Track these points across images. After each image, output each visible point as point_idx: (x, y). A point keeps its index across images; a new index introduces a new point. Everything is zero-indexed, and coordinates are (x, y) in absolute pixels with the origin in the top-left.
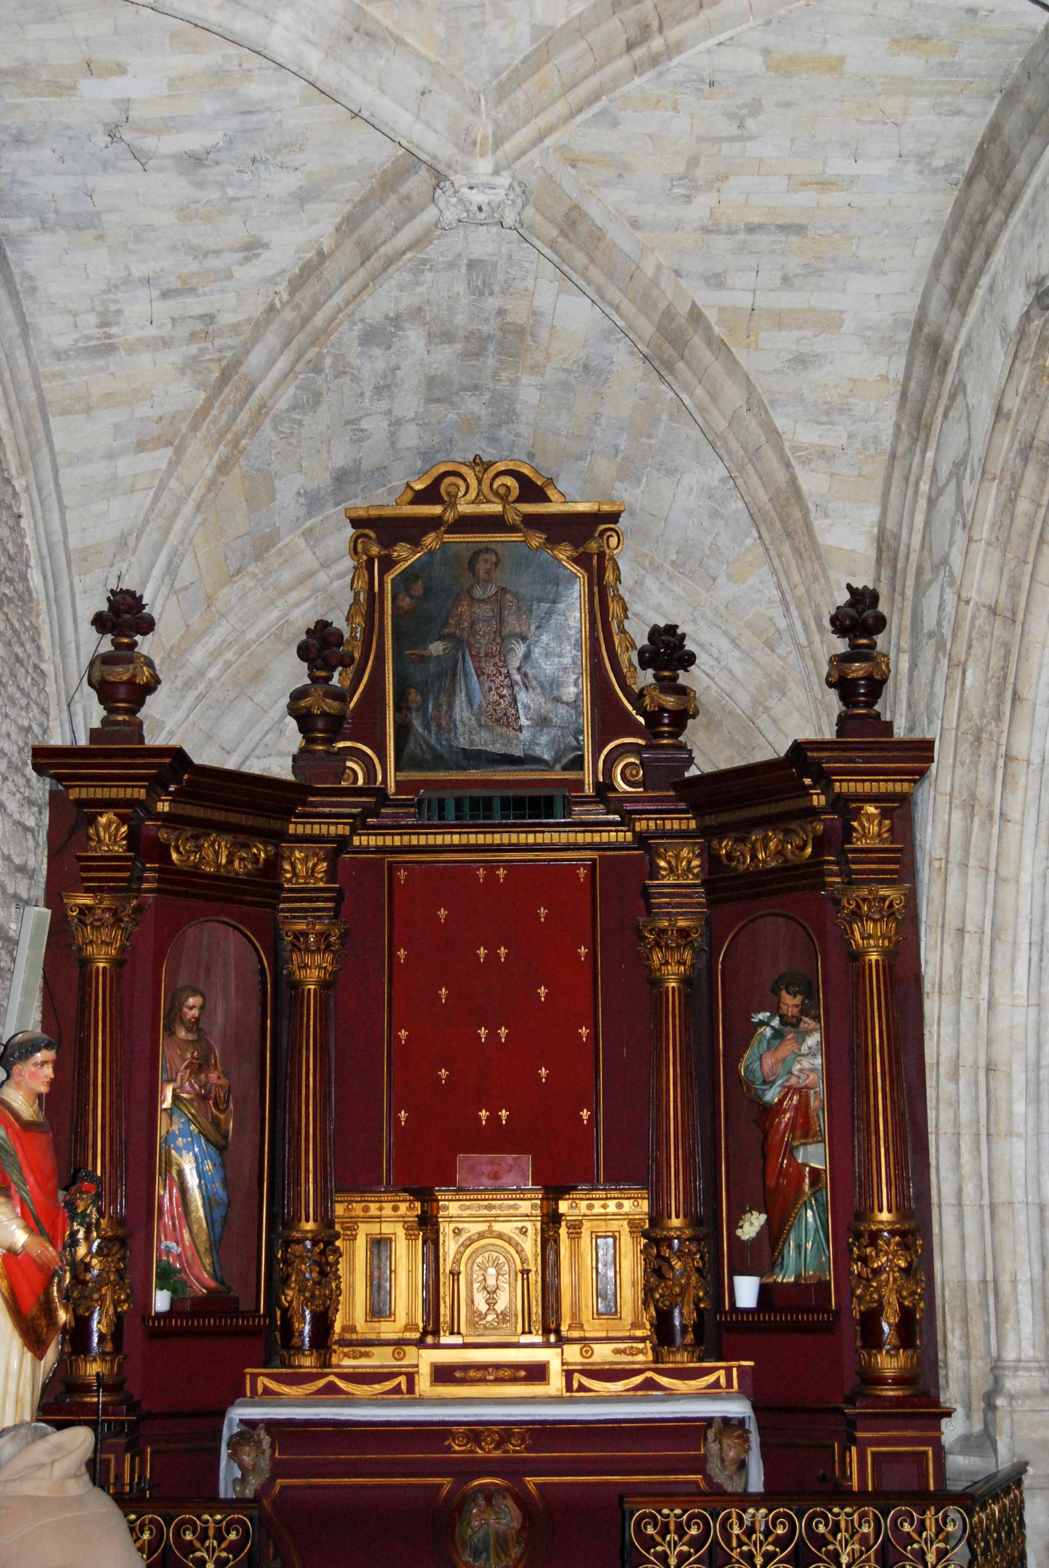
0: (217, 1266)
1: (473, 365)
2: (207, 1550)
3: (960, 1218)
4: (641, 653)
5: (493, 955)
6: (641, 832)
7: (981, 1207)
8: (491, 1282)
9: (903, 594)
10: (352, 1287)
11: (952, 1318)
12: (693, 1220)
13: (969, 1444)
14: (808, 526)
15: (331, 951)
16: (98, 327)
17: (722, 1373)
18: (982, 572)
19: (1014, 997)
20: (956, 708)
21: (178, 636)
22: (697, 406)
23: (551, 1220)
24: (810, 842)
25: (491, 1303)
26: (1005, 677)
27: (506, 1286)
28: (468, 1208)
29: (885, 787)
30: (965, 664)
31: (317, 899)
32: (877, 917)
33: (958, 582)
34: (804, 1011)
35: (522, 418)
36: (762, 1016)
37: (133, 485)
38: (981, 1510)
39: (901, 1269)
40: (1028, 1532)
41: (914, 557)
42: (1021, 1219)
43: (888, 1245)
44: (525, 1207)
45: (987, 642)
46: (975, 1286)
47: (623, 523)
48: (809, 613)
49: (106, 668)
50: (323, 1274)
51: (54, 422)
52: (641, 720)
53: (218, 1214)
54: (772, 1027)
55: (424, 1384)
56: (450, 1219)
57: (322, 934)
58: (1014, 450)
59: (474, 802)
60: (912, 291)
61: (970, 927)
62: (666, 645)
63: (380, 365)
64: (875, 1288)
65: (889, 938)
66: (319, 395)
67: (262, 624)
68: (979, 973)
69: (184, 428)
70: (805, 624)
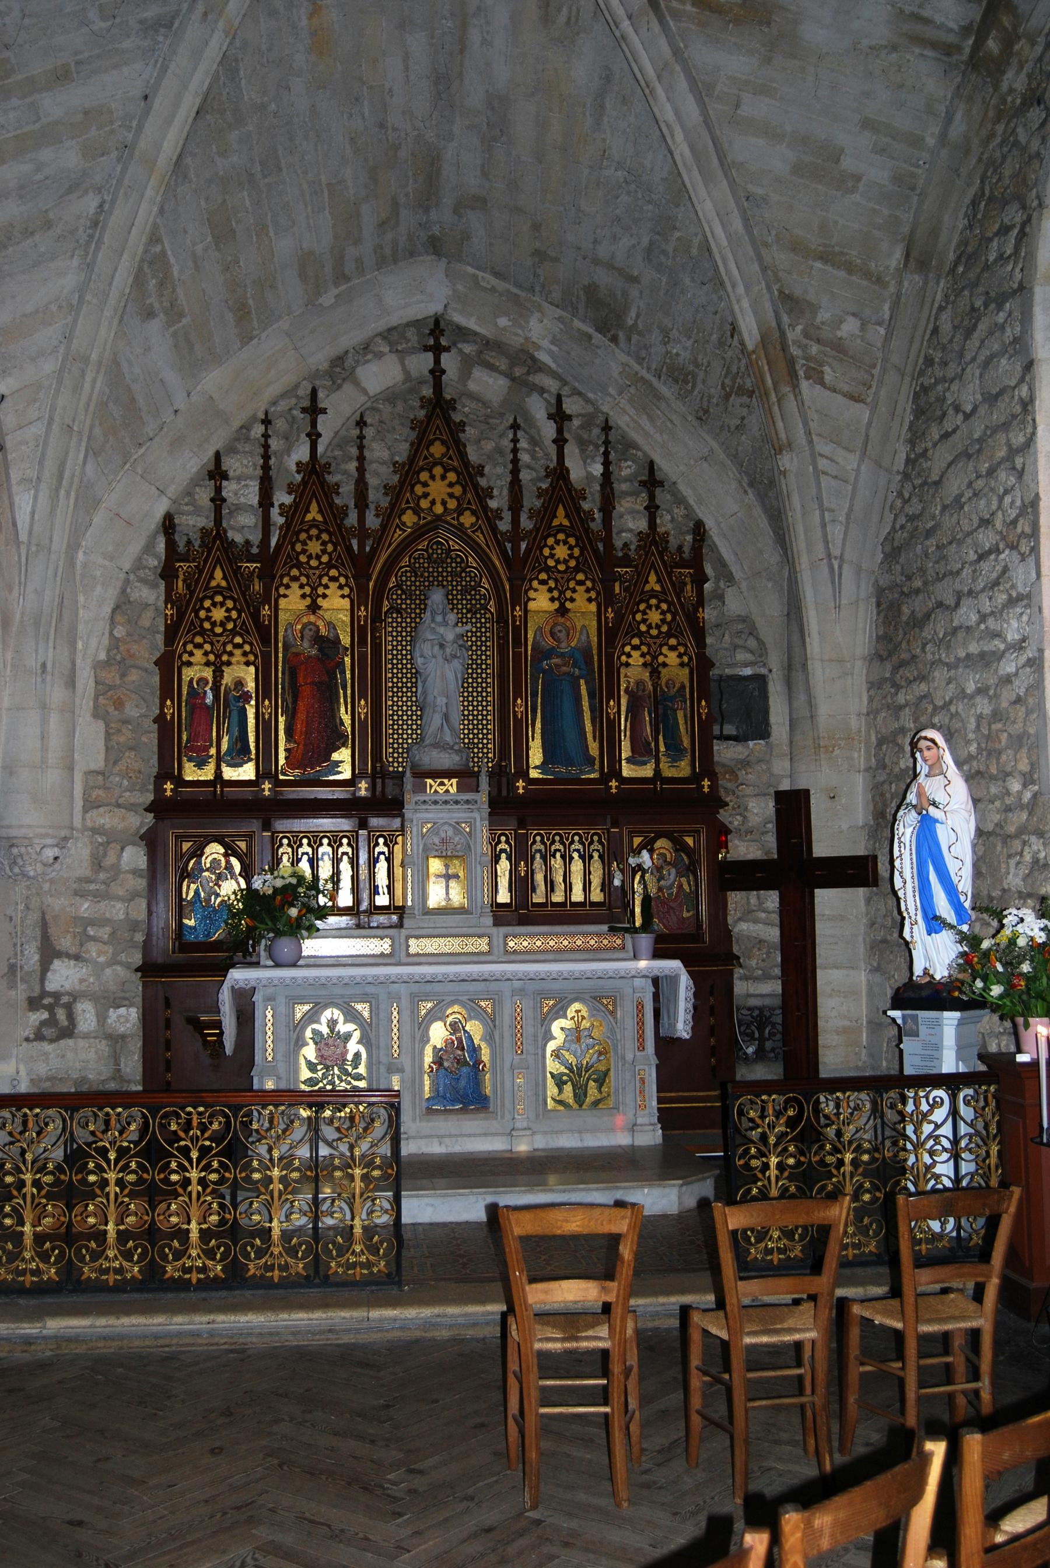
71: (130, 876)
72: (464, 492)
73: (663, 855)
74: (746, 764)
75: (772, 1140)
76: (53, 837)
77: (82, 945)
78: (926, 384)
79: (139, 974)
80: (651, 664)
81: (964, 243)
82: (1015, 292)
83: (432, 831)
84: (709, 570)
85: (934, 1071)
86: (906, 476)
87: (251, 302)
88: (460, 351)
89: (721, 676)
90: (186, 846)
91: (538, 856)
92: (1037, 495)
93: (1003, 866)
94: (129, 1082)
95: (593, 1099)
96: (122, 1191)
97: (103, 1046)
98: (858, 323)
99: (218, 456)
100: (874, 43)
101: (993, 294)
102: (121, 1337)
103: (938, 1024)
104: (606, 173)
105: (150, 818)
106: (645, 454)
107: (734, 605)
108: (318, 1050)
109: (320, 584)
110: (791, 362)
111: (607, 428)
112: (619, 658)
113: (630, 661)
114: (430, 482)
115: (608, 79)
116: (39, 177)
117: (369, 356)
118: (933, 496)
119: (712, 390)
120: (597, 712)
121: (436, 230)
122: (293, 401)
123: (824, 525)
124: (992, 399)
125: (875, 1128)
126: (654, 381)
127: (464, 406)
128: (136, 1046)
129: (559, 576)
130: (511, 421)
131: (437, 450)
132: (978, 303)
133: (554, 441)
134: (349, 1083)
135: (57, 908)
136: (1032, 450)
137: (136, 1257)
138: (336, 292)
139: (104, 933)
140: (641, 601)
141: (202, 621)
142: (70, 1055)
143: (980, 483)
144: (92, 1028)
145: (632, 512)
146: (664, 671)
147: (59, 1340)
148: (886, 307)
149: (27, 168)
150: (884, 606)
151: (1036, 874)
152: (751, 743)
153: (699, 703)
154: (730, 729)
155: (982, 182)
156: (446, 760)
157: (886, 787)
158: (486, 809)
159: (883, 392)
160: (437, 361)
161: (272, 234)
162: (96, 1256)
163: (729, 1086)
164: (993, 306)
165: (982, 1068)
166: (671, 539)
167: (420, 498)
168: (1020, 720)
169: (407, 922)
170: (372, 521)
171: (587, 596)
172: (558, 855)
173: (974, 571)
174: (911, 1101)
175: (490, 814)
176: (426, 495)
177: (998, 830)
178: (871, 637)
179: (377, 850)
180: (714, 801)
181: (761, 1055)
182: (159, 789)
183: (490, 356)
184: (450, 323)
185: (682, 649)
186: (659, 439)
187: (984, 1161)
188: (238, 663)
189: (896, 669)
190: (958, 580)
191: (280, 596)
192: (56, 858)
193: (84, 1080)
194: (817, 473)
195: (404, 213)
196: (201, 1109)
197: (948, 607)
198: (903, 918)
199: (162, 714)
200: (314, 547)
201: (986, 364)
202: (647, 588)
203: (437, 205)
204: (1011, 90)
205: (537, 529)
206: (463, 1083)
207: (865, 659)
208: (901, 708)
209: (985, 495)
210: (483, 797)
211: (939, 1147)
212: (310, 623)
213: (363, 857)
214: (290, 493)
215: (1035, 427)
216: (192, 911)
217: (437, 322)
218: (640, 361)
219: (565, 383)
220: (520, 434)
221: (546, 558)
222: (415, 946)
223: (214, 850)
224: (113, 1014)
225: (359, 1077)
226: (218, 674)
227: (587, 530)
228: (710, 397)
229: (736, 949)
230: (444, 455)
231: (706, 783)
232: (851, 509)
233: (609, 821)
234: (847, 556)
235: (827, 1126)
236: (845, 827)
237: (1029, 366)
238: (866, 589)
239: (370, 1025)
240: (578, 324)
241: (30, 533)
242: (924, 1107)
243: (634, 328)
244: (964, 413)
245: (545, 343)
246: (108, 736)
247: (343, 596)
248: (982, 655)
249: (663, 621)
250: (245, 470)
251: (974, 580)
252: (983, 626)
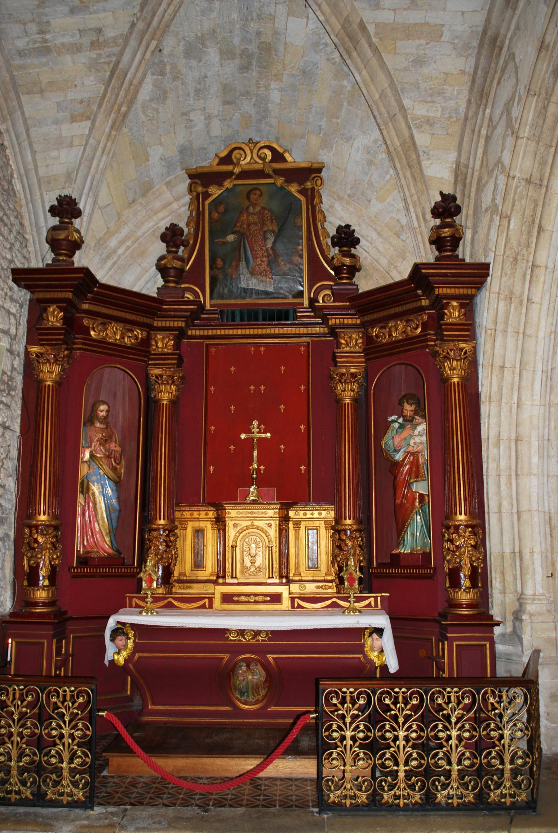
0: (114, 542)
1: (245, 77)
2: (66, 707)
3: (500, 519)
4: (333, 238)
5: (257, 390)
6: (332, 325)
7: (512, 513)
8: (253, 551)
9: (469, 197)
10: (184, 553)
11: (495, 571)
12: (359, 521)
13: (508, 638)
14: (419, 163)
15: (175, 385)
16: (39, 33)
17: (372, 599)
18: (523, 158)
19: (533, 400)
20: (504, 243)
21: (103, 233)
22: (363, 82)
23: (284, 520)
24: (420, 326)
25: (253, 562)
26: (533, 221)
27: (261, 553)
28: (241, 513)
29: (462, 291)
30: (510, 216)
31: (168, 359)
32: (458, 358)
33: (508, 169)
34: (416, 413)
35: (272, 114)
36: (394, 417)
37: (72, 142)
38: (360, 578)
39: (472, 546)
40: (540, 688)
41: (476, 174)
42: (536, 519)
43: (465, 533)
44: (270, 513)
45: (523, 202)
46: (508, 555)
47: (323, 174)
48: (419, 210)
49: (54, 232)
50: (168, 546)
51: (24, 98)
52: (333, 273)
53: (114, 516)
54: (399, 423)
55: (217, 602)
56: (232, 519)
57: (170, 376)
58: (549, 72)
59: (249, 313)
60: (482, 9)
61: (507, 365)
62: (345, 233)
63: (197, 74)
64: (458, 556)
65: (465, 370)
66: (165, 92)
67: (144, 228)
68: (512, 389)
69: (95, 107)
70: (417, 216)
75: (453, 720)
137: (81, 786)
162: (56, 783)
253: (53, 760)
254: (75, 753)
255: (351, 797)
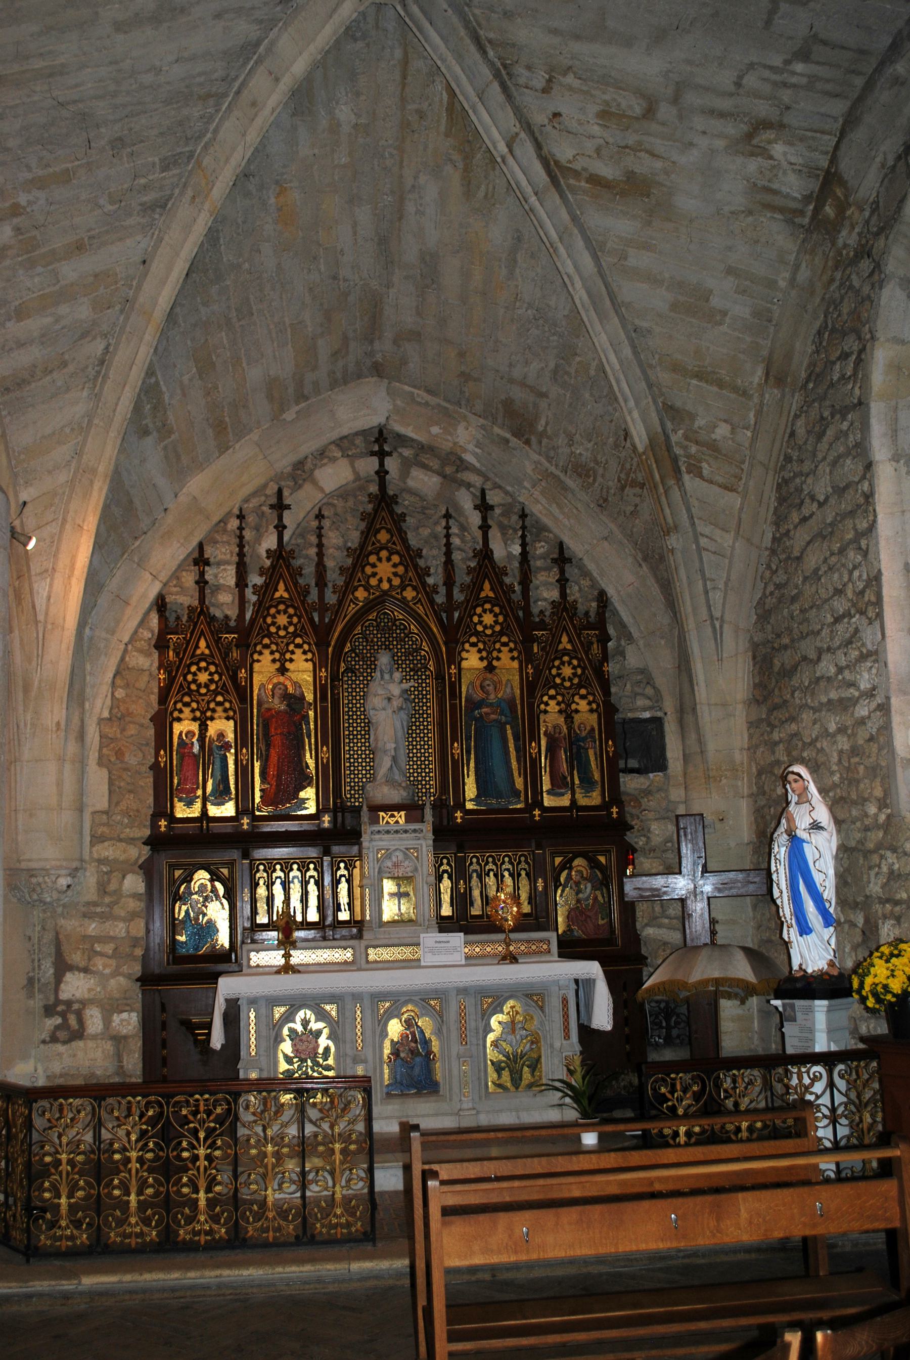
71: (131, 900)
72: (406, 571)
73: (581, 872)
74: (647, 792)
76: (66, 868)
77: (89, 959)
78: (786, 477)
79: (139, 984)
80: (565, 711)
81: (812, 364)
82: (855, 406)
83: (388, 856)
84: (611, 631)
85: (810, 1051)
86: (773, 552)
87: (227, 419)
88: (401, 454)
89: (624, 719)
90: (178, 873)
91: (475, 875)
92: (880, 571)
93: (865, 876)
94: (130, 1076)
95: (527, 1082)
96: (141, 1167)
97: (109, 1046)
98: (729, 427)
99: (201, 546)
100: (733, 209)
101: (837, 407)
102: (144, 1291)
103: (810, 1011)
104: (520, 312)
105: (146, 850)
106: (555, 536)
107: (633, 659)
108: (294, 1045)
109: (288, 651)
110: (675, 460)
111: (523, 516)
112: (538, 706)
113: (548, 708)
114: (378, 564)
115: (519, 239)
116: (57, 327)
117: (325, 461)
118: (796, 569)
119: (610, 483)
120: (521, 751)
121: (379, 357)
122: (263, 498)
123: (706, 592)
124: (840, 491)
125: (766, 1098)
126: (562, 476)
127: (404, 500)
128: (136, 1045)
129: (487, 639)
130: (444, 512)
131: (383, 537)
132: (826, 414)
133: (480, 528)
134: (320, 1073)
135: (69, 928)
136: (874, 534)
137: (154, 1223)
138: (297, 408)
139: (109, 949)
140: (556, 658)
141: (189, 683)
142: (80, 1054)
143: (834, 559)
144: (99, 1031)
145: (546, 584)
146: (577, 717)
147: (94, 1294)
148: (752, 415)
149: (48, 320)
150: (759, 659)
151: (892, 883)
152: (651, 775)
153: (607, 743)
154: (633, 763)
155: (825, 316)
156: (395, 796)
157: (766, 810)
158: (430, 836)
159: (751, 483)
160: (382, 464)
161: (244, 365)
163: (643, 1067)
164: (838, 416)
165: (861, 1046)
166: (579, 605)
167: (369, 577)
168: (874, 755)
169: (366, 935)
170: (331, 598)
171: (510, 655)
172: (491, 874)
173: (832, 631)
174: (795, 1076)
175: (434, 841)
176: (374, 575)
177: (860, 847)
178: (748, 684)
179: (339, 873)
180: (623, 826)
181: (669, 1041)
182: (154, 826)
183: (425, 458)
184: (392, 431)
185: (591, 698)
186: (567, 523)
187: (858, 1125)
188: (220, 718)
189: (771, 711)
190: (818, 638)
191: (254, 661)
192: (69, 886)
193: (93, 1075)
194: (699, 549)
195: (352, 345)
196: (207, 1096)
197: (811, 661)
198: (782, 923)
199: (157, 763)
200: (282, 620)
201: (834, 463)
202: (561, 647)
203: (379, 338)
204: (845, 246)
205: (467, 601)
206: (417, 1070)
207: (744, 703)
208: (776, 744)
209: (838, 570)
210: (427, 828)
211: (820, 1115)
212: (279, 683)
213: (327, 880)
214: (261, 575)
215: (875, 516)
216: (183, 929)
217: (381, 432)
218: (549, 459)
219: (487, 479)
220: (451, 522)
221: (476, 624)
222: (373, 954)
223: (202, 877)
224: (116, 1018)
225: (328, 1068)
226: (203, 728)
227: (509, 601)
228: (608, 488)
229: (644, 951)
230: (388, 541)
231: (615, 810)
232: (728, 579)
233: (533, 845)
234: (727, 617)
235: (726, 1098)
236: (733, 844)
237: (869, 466)
238: (743, 644)
239: (337, 1023)
240: (497, 430)
241: (47, 614)
242: (807, 1081)
243: (543, 434)
244: (819, 501)
245: (471, 447)
246: (111, 783)
247: (307, 660)
248: (841, 700)
249: (575, 675)
250: (223, 557)
251: (831, 639)
252: (840, 677)
253: (185, 1190)
254: (214, 1178)
255: (207, 1233)
